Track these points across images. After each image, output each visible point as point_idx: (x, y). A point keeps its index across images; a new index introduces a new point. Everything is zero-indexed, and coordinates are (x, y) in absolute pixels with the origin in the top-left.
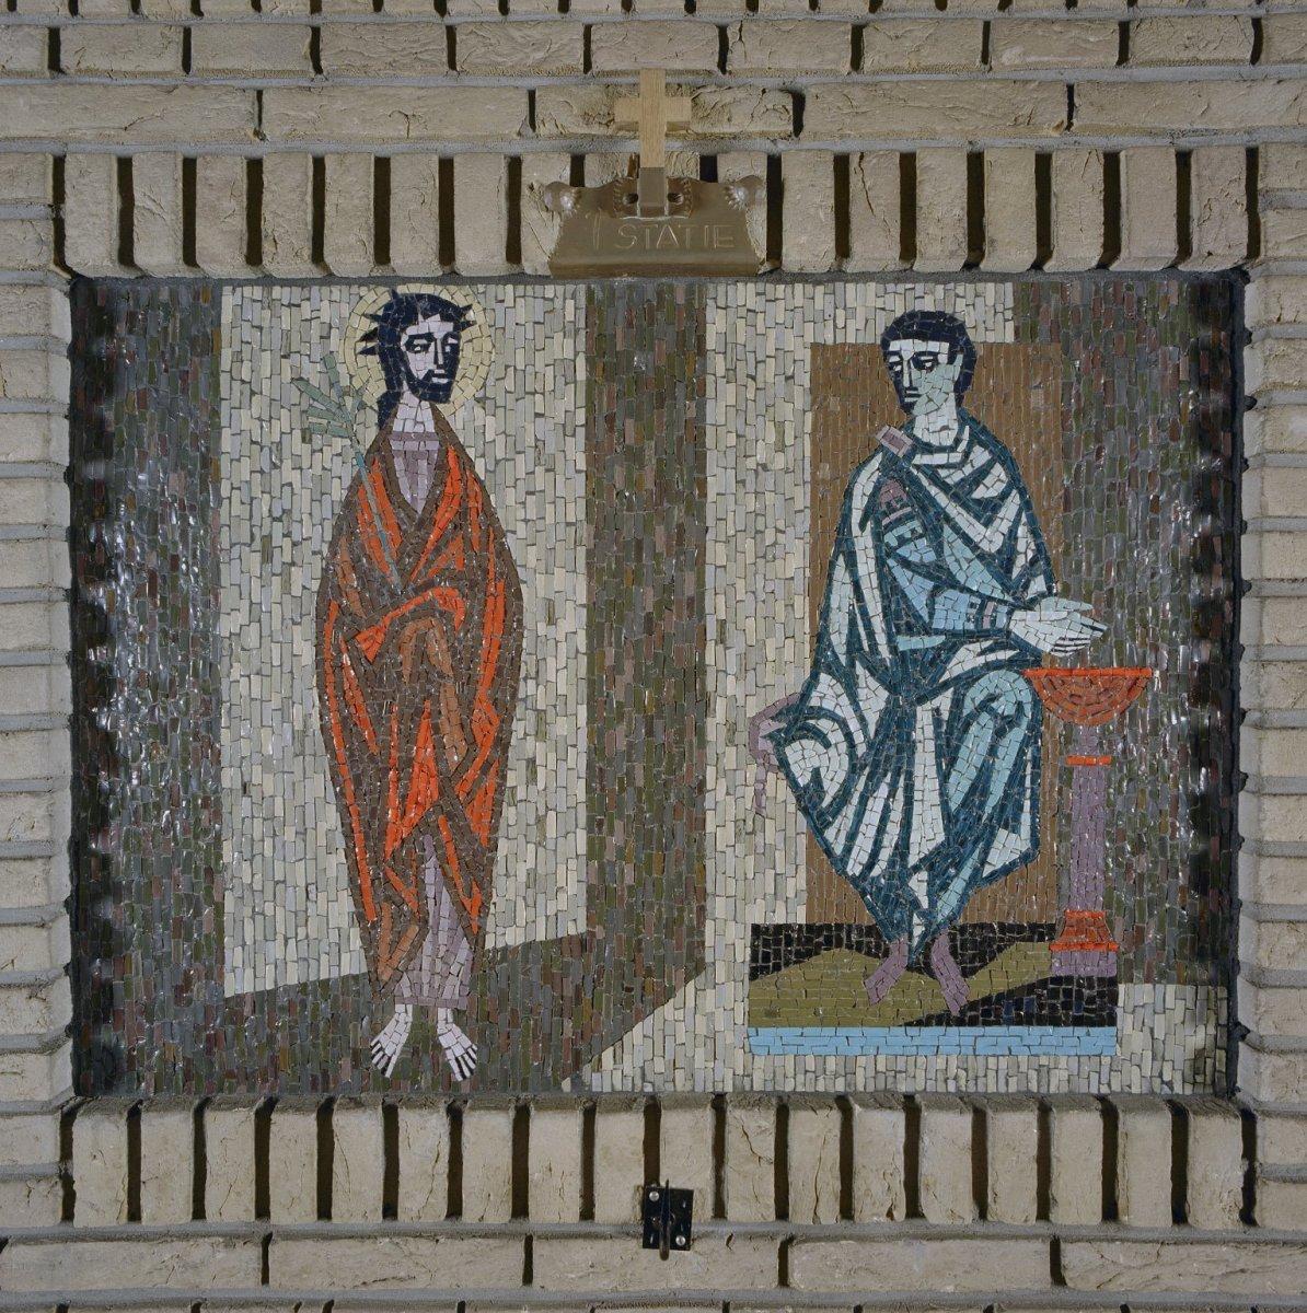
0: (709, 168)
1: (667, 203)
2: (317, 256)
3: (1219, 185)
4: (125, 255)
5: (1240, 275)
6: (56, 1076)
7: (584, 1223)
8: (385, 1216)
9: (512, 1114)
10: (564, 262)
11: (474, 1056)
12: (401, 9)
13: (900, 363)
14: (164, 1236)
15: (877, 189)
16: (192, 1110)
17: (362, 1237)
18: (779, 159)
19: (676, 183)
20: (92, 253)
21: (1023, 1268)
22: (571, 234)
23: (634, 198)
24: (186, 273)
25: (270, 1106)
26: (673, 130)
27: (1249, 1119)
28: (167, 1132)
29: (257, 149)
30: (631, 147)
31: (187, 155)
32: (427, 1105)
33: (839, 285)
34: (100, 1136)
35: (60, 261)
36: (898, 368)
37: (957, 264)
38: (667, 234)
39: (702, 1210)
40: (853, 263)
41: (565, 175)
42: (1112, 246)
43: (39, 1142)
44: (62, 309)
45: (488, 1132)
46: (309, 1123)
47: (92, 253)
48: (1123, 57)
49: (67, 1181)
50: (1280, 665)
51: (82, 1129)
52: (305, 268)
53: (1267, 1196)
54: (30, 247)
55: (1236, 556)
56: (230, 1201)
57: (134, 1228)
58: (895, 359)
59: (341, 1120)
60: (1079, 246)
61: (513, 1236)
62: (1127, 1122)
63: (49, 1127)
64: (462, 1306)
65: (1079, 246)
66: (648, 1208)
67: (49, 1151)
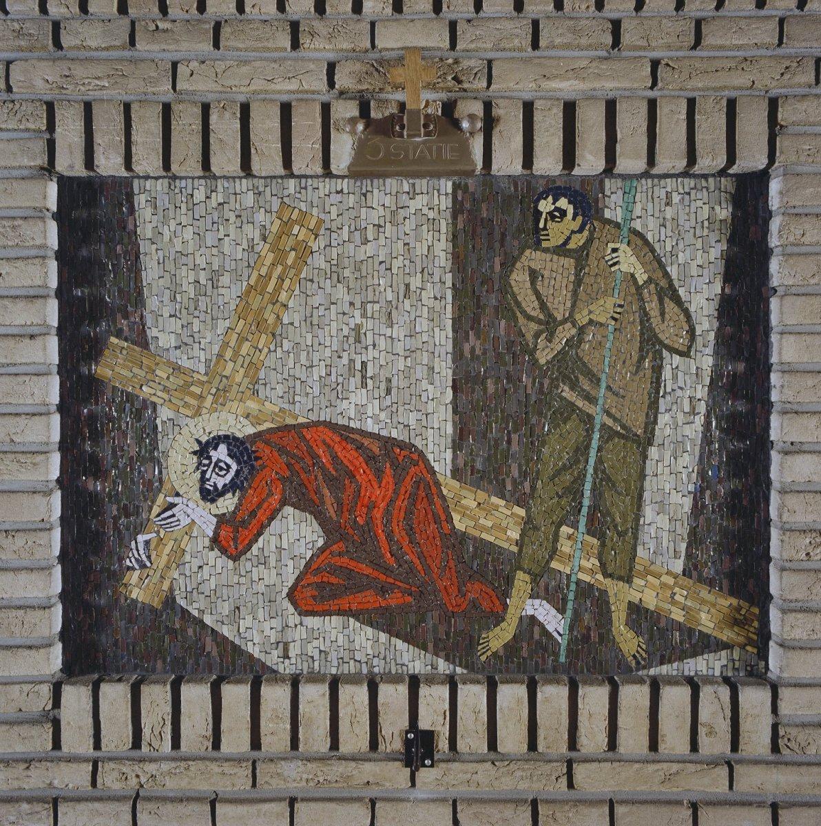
1: (422, 129)
3: (753, 126)
4: (89, 162)
5: (762, 177)
6: (55, 658)
8: (94, 749)
11: (644, 655)
12: (493, 9)
14: (353, 758)
15: (266, 127)
17: (756, 762)
20: (70, 162)
22: (361, 150)
23: (402, 127)
24: (125, 174)
28: (156, 698)
30: (400, 96)
33: (327, 180)
34: (76, 698)
39: (443, 744)
40: (735, 167)
41: (356, 113)
44: (53, 189)
45: (634, 697)
47: (70, 162)
49: (56, 724)
50: (23, 416)
55: (768, 354)
56: (236, 739)
57: (57, 753)
62: (424, 691)
63: (46, 690)
66: (408, 743)
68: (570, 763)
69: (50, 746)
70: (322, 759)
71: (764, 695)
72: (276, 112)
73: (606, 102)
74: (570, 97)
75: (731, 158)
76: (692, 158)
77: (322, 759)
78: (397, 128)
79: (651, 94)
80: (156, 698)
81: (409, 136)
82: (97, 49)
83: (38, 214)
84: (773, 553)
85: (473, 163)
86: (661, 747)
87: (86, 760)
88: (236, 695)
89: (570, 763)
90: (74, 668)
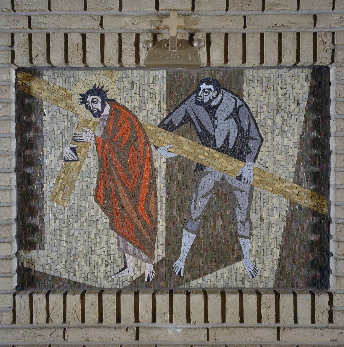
0: (192, 35)
2: (84, 61)
18: (67, 34)
19: (181, 41)
21: (128, 337)
22: (149, 57)
23: (168, 45)
25: (49, 292)
26: (179, 27)
27: (331, 295)
29: (102, 31)
31: (261, 32)
34: (23, 300)
35: (13, 61)
37: (276, 64)
38: (177, 56)
40: (299, 63)
46: (166, 297)
48: (85, 9)
51: (17, 297)
53: (336, 315)
54: (5, 58)
59: (141, 296)
61: (274, 328)
63: (11, 297)
64: (50, 346)
67: (10, 303)
68: (279, 328)
69: (220, 321)
71: (326, 298)
74: (245, 15)
75: (315, 60)
79: (244, 31)
80: (162, 300)
81: (172, 49)
82: (164, 10)
87: (274, 328)
88: (74, 300)
89: (279, 328)
90: (21, 288)
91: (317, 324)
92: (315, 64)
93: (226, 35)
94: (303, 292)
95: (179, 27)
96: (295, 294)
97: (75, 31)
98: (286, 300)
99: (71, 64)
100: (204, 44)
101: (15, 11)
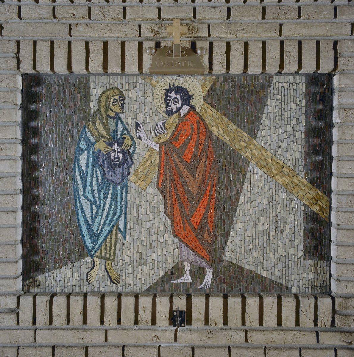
7: (261, 326)
9: (152, 297)
10: (152, 71)
13: (170, 100)
15: (114, 51)
16: (17, 297)
19: (184, 48)
20: (27, 67)
23: (172, 52)
26: (182, 35)
27: (333, 299)
29: (70, 39)
32: (271, 295)
35: (18, 68)
36: (169, 101)
40: (284, 71)
42: (246, 67)
43: (11, 303)
44: (19, 79)
45: (216, 303)
49: (18, 314)
52: (100, 70)
56: (307, 320)
57: (85, 327)
58: (168, 98)
59: (158, 300)
60: (237, 68)
63: (15, 299)
65: (237, 68)
67: (13, 305)
70: (274, 330)
71: (329, 301)
72: (224, 45)
73: (334, 41)
75: (318, 67)
76: (282, 66)
77: (274, 330)
78: (169, 52)
80: (234, 303)
81: (175, 56)
83: (13, 91)
84: (333, 238)
85: (204, 68)
86: (71, 322)
88: (270, 302)
91: (22, 325)
92: (319, 72)
93: (300, 43)
94: (251, 296)
95: (182, 35)
96: (244, 298)
97: (222, 39)
98: (234, 303)
99: (110, 71)
100: (206, 51)
101: (21, 19)
